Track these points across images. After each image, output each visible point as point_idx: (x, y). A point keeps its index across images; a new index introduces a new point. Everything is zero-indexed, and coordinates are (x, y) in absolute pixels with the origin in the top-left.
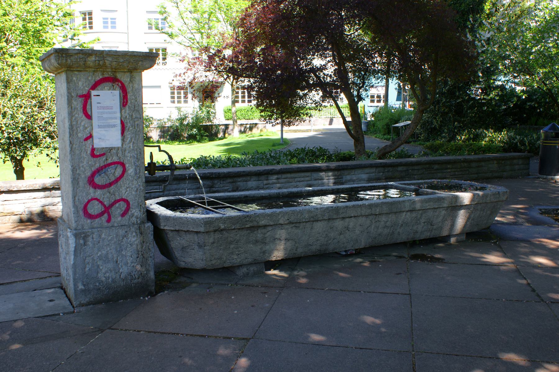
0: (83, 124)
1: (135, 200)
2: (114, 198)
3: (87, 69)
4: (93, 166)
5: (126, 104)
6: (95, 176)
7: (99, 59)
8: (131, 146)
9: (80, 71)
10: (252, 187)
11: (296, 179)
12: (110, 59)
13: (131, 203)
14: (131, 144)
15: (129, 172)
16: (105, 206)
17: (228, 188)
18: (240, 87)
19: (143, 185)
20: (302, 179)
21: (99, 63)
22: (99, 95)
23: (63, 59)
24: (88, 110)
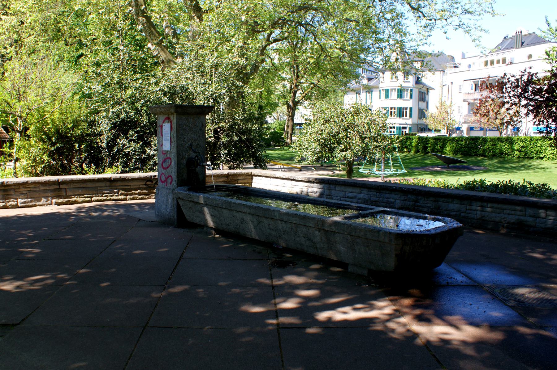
10: (453, 209)
11: (505, 211)
17: (430, 205)
18: (511, 108)
20: (513, 212)
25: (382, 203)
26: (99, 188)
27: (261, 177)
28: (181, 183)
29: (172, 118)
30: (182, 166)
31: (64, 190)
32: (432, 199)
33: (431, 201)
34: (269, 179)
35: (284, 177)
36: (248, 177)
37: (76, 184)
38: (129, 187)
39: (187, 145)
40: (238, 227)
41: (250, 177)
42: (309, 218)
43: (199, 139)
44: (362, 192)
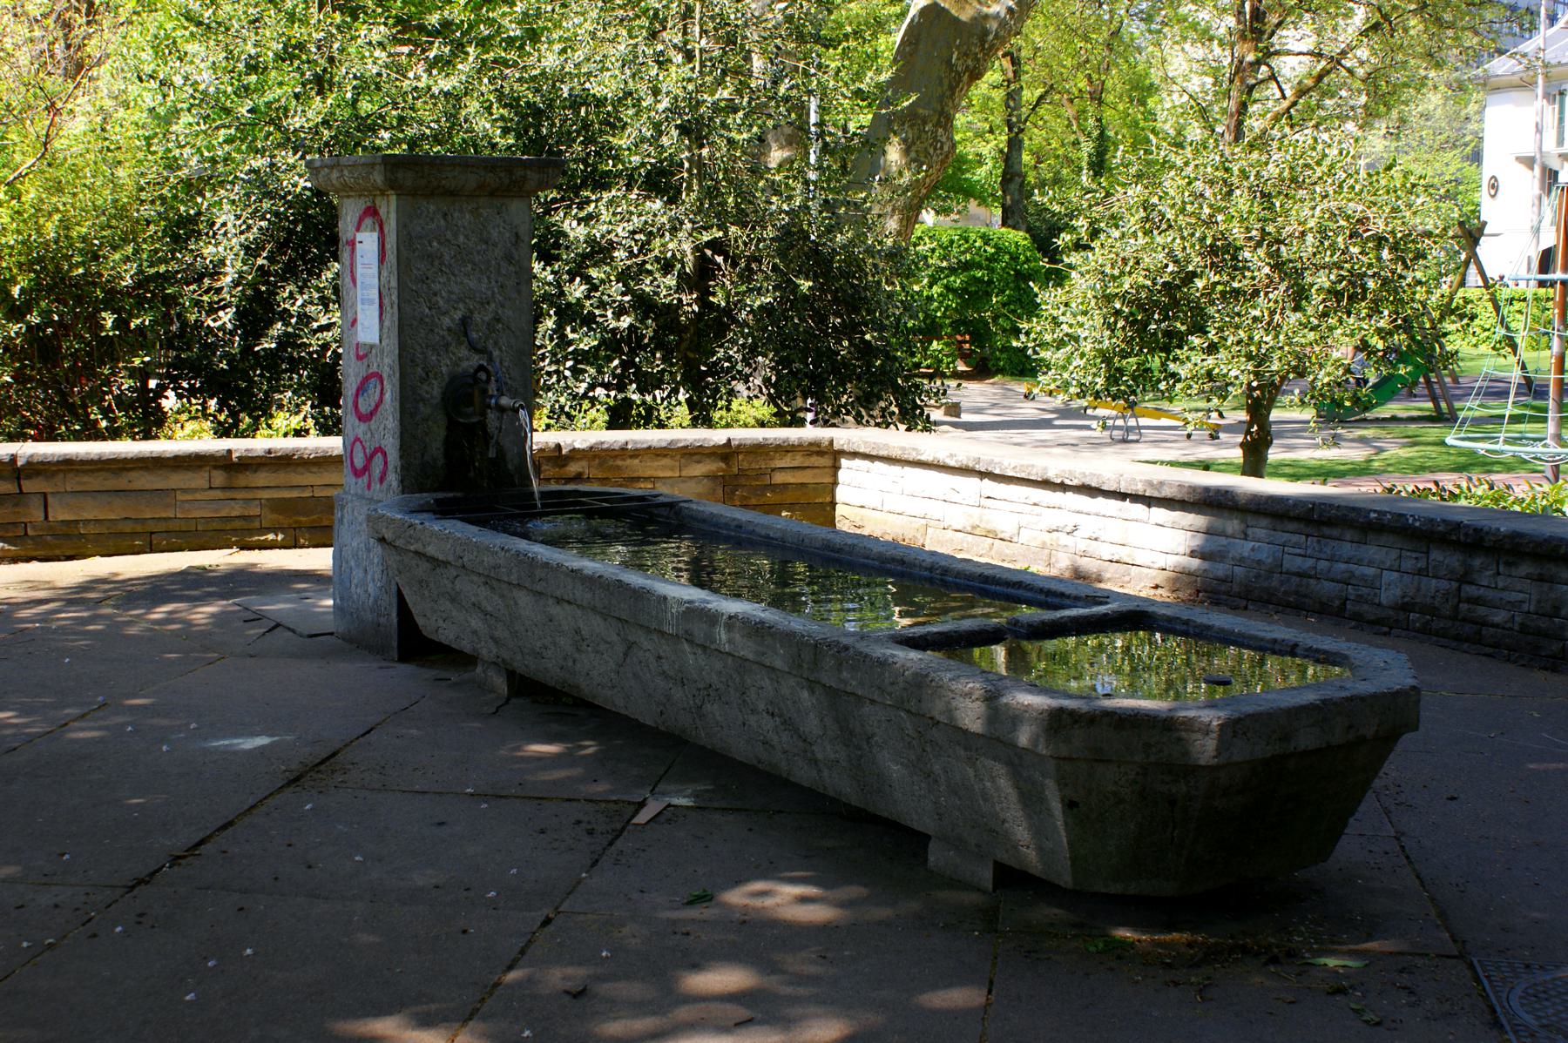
17: (1521, 596)
25: (1327, 584)
26: (180, 496)
27: (866, 463)
28: (416, 476)
29: (382, 212)
30: (424, 410)
31: (37, 502)
32: (1525, 568)
33: (1527, 577)
34: (896, 469)
35: (952, 463)
36: (816, 461)
37: (86, 479)
38: (307, 494)
39: (446, 321)
40: (570, 664)
41: (826, 461)
42: (771, 635)
43: (499, 298)
44: (1250, 531)
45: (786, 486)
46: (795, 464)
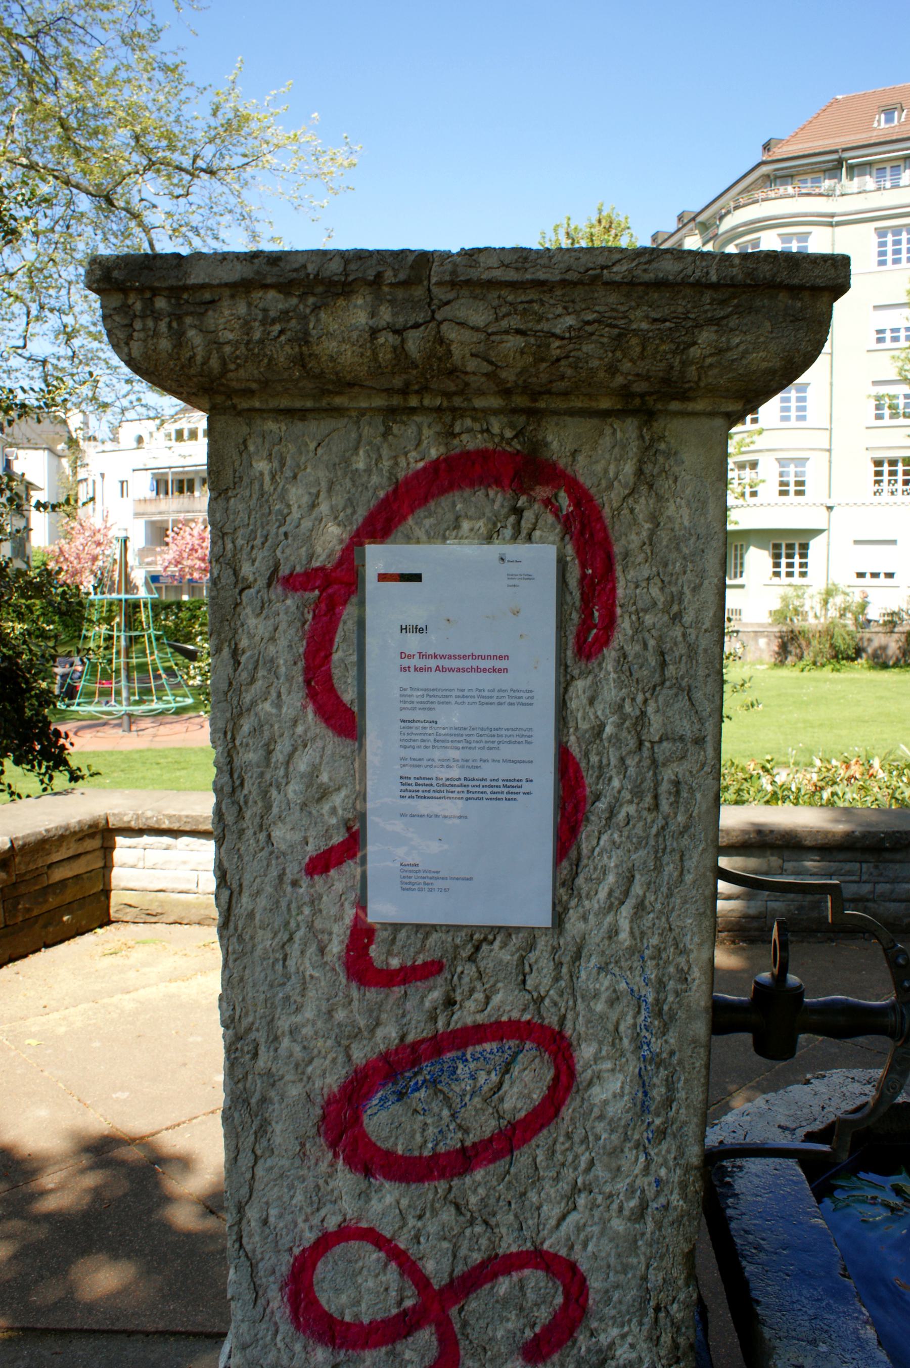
0: (302, 764)
1: (625, 1269)
2: (484, 1242)
3: (338, 401)
4: (356, 1035)
5: (604, 640)
6: (369, 1096)
7: (401, 321)
8: (625, 925)
9: (301, 414)
12: (479, 316)
13: (595, 1284)
14: (626, 911)
15: (599, 1094)
16: (421, 1281)
19: (683, 1186)
21: (400, 352)
22: (417, 578)
23: (156, 334)
24: (336, 672)
41: (96, 843)
45: (63, 882)
46: (71, 853)
